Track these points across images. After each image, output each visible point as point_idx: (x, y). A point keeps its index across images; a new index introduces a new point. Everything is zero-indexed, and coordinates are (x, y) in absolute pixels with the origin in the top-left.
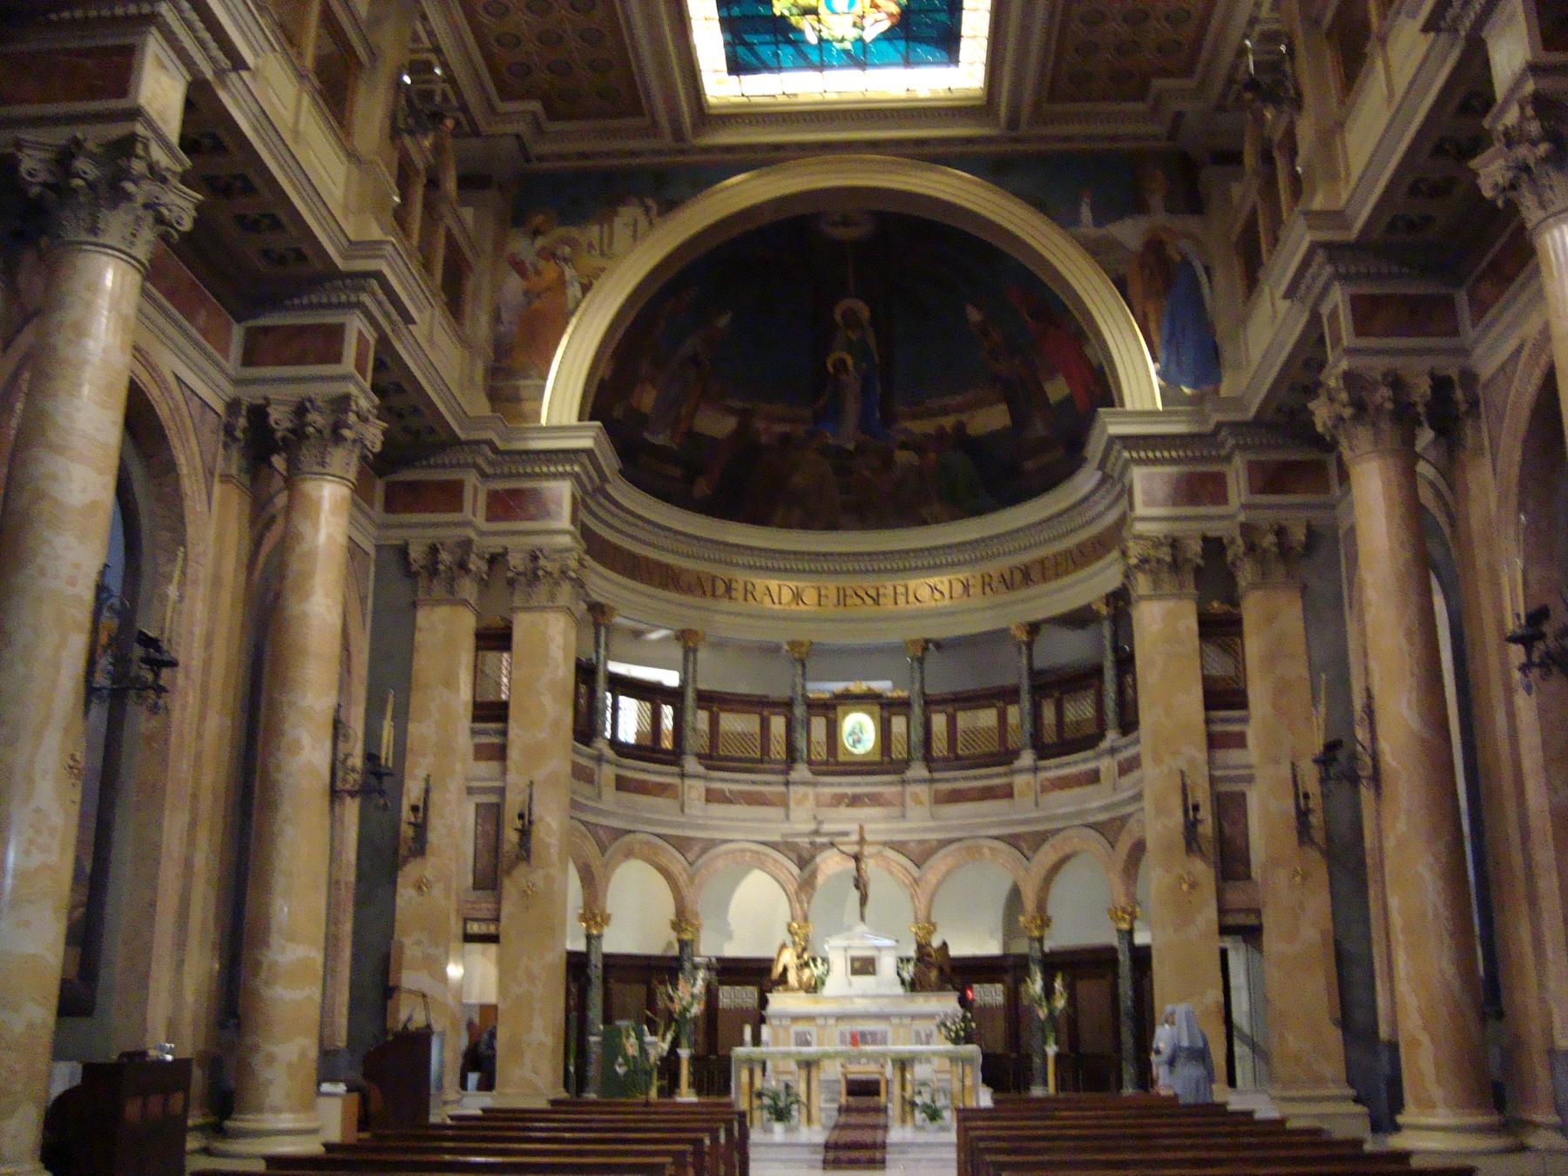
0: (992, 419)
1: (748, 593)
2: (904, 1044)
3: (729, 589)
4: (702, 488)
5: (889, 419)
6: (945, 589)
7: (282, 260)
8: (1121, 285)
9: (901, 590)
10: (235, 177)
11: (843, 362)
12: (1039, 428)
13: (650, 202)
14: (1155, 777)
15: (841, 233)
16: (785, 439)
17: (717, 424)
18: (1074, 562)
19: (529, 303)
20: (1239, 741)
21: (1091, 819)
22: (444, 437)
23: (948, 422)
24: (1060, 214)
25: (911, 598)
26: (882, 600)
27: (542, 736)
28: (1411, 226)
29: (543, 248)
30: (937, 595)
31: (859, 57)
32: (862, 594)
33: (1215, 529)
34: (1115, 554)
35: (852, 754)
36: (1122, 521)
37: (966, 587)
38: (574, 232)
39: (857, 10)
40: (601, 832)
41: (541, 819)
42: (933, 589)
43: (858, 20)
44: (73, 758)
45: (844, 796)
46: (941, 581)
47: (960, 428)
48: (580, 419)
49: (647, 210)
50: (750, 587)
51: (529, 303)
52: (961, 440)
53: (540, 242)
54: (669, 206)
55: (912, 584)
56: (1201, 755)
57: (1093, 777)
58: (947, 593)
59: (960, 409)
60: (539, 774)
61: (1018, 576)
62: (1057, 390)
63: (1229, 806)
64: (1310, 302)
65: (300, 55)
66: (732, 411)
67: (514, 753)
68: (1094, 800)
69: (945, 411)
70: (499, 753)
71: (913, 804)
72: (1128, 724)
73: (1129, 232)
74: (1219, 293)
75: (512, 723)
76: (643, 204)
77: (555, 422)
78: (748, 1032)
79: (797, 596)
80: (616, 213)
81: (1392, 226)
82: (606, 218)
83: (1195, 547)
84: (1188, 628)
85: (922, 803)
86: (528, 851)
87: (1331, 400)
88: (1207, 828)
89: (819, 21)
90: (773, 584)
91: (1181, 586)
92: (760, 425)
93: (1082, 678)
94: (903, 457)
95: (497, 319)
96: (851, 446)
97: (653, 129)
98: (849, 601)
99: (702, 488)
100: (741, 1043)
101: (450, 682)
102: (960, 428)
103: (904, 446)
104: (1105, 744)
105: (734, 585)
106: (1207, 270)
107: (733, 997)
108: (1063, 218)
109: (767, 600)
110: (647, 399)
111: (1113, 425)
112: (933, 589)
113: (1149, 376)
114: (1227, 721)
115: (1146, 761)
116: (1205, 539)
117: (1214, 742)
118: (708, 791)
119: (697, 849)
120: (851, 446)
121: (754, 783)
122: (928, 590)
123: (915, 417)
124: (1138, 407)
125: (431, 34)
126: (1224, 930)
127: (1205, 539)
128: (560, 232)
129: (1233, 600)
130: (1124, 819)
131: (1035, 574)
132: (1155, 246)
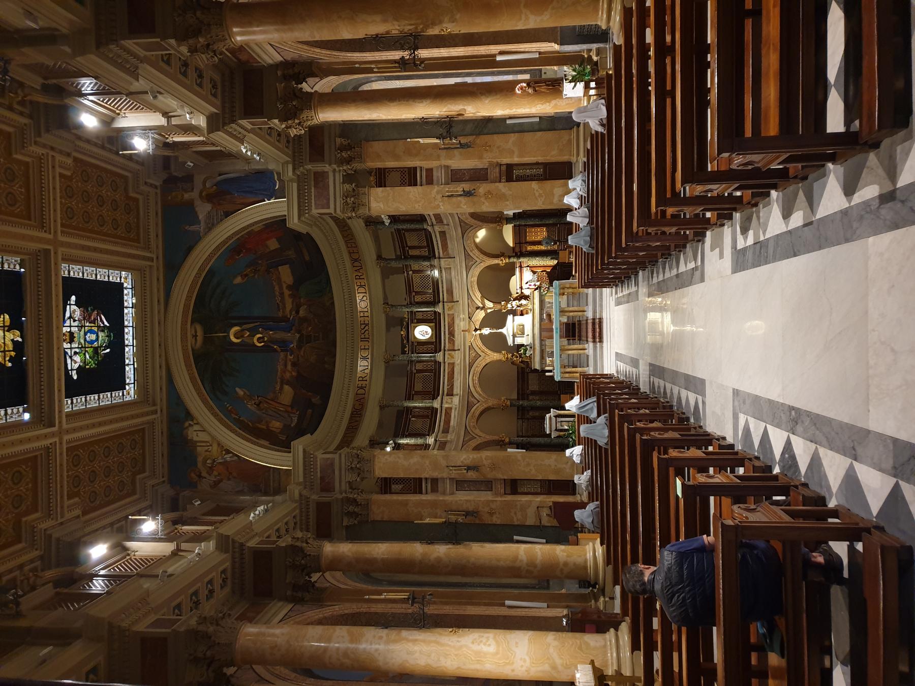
0: (286, 274)
1: (363, 379)
2: (105, 683)
3: (362, 388)
4: (316, 400)
5: (285, 319)
6: (362, 295)
7: (224, 580)
8: (227, 214)
9: (362, 314)
10: (191, 599)
11: (259, 339)
12: (291, 253)
13: (187, 424)
14: (444, 208)
15: (200, 339)
16: (294, 364)
17: (287, 394)
18: (352, 239)
19: (235, 478)
20: (430, 171)
21: (460, 235)
22: (298, 511)
23: (287, 292)
24: (193, 241)
25: (366, 310)
26: (367, 322)
27: (427, 462)
28: (215, 87)
29: (208, 473)
30: (365, 298)
31: (117, 328)
32: (363, 331)
33: (339, 178)
34: (349, 221)
35: (432, 334)
36: (336, 219)
37: (361, 286)
38: (200, 459)
39: (96, 329)
40: (466, 439)
41: (462, 462)
42: (361, 300)
43: (100, 329)
44: (451, 632)
45: (449, 338)
46: (359, 297)
47: (289, 287)
48: (290, 452)
49: (190, 425)
50: (361, 379)
51: (235, 478)
52: (294, 288)
53: (204, 474)
54: (189, 415)
55: (359, 309)
56: (435, 189)
57: (443, 234)
58: (363, 294)
59: (281, 288)
60: (444, 463)
61: (356, 264)
62: (273, 244)
63: (456, 176)
64: (245, 133)
65: (225, 520)
66: (281, 388)
67: (435, 475)
68: (454, 233)
69: (282, 294)
70: (435, 481)
71: (453, 310)
72: (421, 219)
73: (203, 210)
74: (236, 169)
75: (422, 476)
76: (187, 428)
77: (291, 463)
78: (547, 374)
79: (364, 358)
80: (192, 440)
81: (215, 95)
82: (193, 444)
83: (347, 186)
84: (382, 191)
85: (452, 306)
86: (475, 467)
87: (290, 127)
88: (467, 186)
89: (101, 346)
90: (359, 369)
91: (364, 194)
92: (288, 375)
93: (400, 236)
94: (302, 313)
95: (241, 493)
96: (298, 335)
97: (152, 423)
98: (367, 336)
99: (316, 400)
100: (552, 377)
101: (405, 504)
102: (289, 287)
103: (297, 312)
104: (430, 228)
105: (360, 385)
106: (220, 175)
107: (533, 385)
108: (197, 239)
109: (366, 371)
110: (276, 425)
111: (294, 223)
112: (361, 300)
113: (271, 203)
114: (421, 176)
115: (437, 211)
116: (344, 183)
117: (430, 181)
118: (448, 395)
119: (472, 399)
120: (298, 335)
121: (444, 376)
122: (362, 302)
123: (284, 307)
124: (286, 209)
125: (32, 561)
126: (500, 182)
127: (344, 183)
128: (200, 465)
129: (370, 172)
130: (461, 221)
131: (355, 256)
132: (209, 198)
